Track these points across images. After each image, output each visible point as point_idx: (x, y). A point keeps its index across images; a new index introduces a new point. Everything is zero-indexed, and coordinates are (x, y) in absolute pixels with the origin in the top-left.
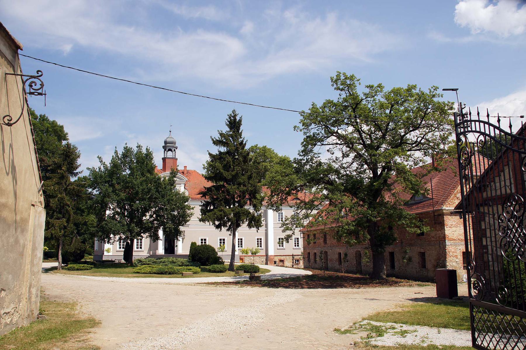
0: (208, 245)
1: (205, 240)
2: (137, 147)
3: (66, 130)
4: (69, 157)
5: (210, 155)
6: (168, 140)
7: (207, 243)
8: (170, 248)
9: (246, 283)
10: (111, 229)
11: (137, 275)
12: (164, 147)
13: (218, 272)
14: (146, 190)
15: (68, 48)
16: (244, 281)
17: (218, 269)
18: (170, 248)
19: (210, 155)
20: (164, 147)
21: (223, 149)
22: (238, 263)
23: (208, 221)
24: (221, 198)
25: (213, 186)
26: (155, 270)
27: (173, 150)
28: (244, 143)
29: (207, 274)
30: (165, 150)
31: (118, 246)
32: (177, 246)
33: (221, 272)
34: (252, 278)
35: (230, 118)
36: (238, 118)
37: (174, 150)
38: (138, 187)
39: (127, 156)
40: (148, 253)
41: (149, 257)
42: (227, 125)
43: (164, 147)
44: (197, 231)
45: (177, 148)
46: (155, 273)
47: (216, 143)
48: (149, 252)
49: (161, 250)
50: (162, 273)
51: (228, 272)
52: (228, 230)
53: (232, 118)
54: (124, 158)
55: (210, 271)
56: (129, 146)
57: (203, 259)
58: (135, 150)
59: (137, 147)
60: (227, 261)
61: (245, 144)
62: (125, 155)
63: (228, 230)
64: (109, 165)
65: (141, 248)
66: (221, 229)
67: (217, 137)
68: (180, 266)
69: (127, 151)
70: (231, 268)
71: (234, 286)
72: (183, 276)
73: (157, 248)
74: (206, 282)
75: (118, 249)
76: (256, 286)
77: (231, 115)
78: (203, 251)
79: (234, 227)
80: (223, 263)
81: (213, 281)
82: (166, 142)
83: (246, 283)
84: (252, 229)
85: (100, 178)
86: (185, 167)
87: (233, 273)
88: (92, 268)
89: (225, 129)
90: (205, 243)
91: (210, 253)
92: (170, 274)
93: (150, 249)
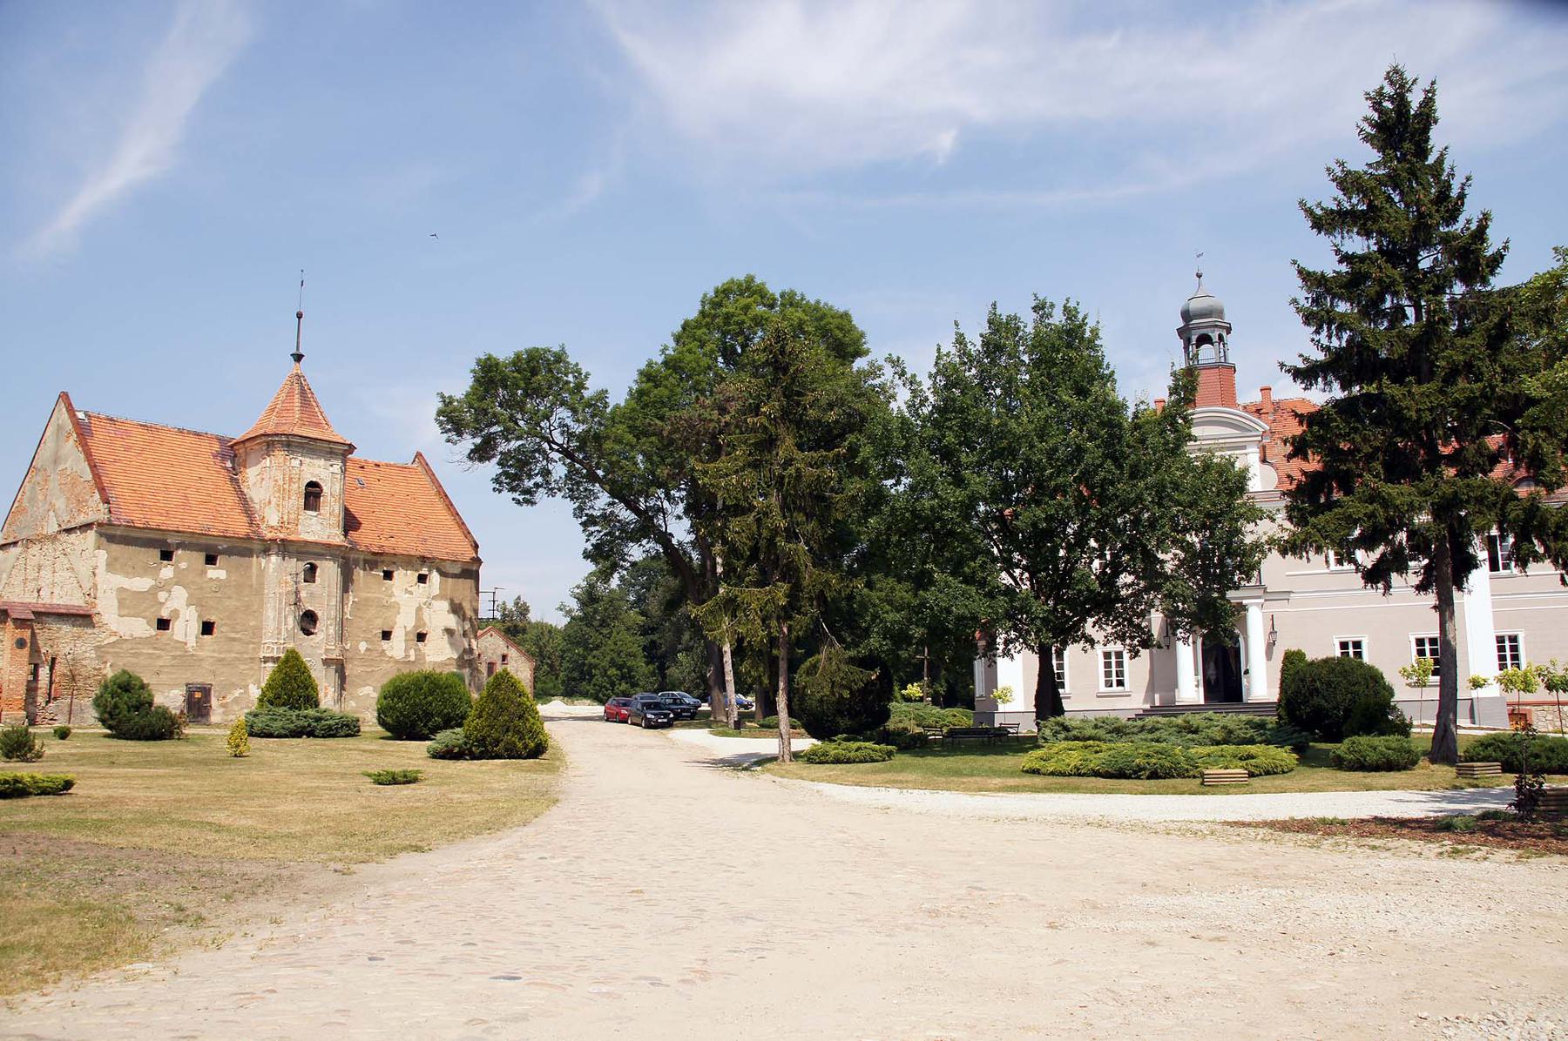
0: (1371, 668)
1: (1357, 645)
2: (1036, 309)
3: (858, 322)
4: (785, 370)
5: (1305, 275)
6: (1195, 305)
7: (1366, 659)
8: (1224, 679)
9: (1490, 831)
10: (949, 612)
11: (1038, 780)
12: (1181, 332)
13: (1376, 768)
14: (1061, 453)
15: (946, 141)
16: (1486, 815)
17: (1372, 757)
18: (1224, 679)
19: (1305, 275)
20: (1181, 332)
21: (1357, 244)
22: (1467, 730)
23: (1319, 550)
24: (1367, 449)
25: (1337, 404)
26: (1095, 761)
27: (1215, 336)
28: (1454, 193)
29: (1323, 775)
30: (1187, 342)
31: (1102, 679)
32: (1247, 672)
33: (1389, 766)
34: (1528, 801)
35: (1377, 106)
36: (1415, 99)
37: (1221, 338)
38: (1032, 447)
39: (999, 348)
40: (1145, 701)
41: (1147, 713)
42: (1368, 138)
43: (1183, 333)
44: (1308, 605)
45: (1229, 330)
46: (1096, 774)
47: (1325, 222)
48: (1149, 696)
49: (1190, 689)
50: (1121, 775)
51: (1424, 768)
52: (1422, 587)
53: (1388, 105)
54: (988, 353)
55: (1339, 764)
56: (1004, 312)
57: (1333, 715)
58: (1028, 322)
59: (1036, 309)
60: (1424, 725)
61: (1462, 196)
62: (993, 347)
63: (1422, 587)
64: (927, 384)
65: (1120, 683)
66: (1388, 587)
67: (1329, 196)
68: (1218, 743)
69: (1001, 333)
70: (1443, 748)
71: (1416, 845)
72: (1207, 786)
73: (1174, 684)
74: (1282, 815)
75: (1103, 688)
76: (1549, 850)
77: (1380, 92)
78: (1329, 684)
79: (1445, 576)
80: (1403, 729)
81: (1300, 815)
82: (1187, 315)
83: (1491, 828)
84: (1533, 568)
85: (901, 430)
86: (1266, 390)
87: (1445, 772)
88: (890, 754)
89: (1364, 157)
90: (1359, 655)
91: (1361, 689)
92: (1154, 775)
93: (1152, 688)
